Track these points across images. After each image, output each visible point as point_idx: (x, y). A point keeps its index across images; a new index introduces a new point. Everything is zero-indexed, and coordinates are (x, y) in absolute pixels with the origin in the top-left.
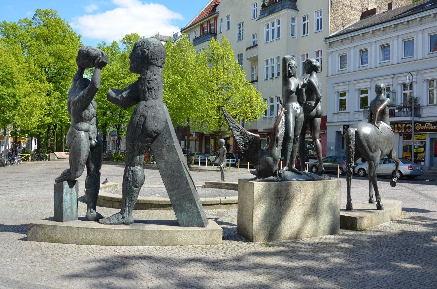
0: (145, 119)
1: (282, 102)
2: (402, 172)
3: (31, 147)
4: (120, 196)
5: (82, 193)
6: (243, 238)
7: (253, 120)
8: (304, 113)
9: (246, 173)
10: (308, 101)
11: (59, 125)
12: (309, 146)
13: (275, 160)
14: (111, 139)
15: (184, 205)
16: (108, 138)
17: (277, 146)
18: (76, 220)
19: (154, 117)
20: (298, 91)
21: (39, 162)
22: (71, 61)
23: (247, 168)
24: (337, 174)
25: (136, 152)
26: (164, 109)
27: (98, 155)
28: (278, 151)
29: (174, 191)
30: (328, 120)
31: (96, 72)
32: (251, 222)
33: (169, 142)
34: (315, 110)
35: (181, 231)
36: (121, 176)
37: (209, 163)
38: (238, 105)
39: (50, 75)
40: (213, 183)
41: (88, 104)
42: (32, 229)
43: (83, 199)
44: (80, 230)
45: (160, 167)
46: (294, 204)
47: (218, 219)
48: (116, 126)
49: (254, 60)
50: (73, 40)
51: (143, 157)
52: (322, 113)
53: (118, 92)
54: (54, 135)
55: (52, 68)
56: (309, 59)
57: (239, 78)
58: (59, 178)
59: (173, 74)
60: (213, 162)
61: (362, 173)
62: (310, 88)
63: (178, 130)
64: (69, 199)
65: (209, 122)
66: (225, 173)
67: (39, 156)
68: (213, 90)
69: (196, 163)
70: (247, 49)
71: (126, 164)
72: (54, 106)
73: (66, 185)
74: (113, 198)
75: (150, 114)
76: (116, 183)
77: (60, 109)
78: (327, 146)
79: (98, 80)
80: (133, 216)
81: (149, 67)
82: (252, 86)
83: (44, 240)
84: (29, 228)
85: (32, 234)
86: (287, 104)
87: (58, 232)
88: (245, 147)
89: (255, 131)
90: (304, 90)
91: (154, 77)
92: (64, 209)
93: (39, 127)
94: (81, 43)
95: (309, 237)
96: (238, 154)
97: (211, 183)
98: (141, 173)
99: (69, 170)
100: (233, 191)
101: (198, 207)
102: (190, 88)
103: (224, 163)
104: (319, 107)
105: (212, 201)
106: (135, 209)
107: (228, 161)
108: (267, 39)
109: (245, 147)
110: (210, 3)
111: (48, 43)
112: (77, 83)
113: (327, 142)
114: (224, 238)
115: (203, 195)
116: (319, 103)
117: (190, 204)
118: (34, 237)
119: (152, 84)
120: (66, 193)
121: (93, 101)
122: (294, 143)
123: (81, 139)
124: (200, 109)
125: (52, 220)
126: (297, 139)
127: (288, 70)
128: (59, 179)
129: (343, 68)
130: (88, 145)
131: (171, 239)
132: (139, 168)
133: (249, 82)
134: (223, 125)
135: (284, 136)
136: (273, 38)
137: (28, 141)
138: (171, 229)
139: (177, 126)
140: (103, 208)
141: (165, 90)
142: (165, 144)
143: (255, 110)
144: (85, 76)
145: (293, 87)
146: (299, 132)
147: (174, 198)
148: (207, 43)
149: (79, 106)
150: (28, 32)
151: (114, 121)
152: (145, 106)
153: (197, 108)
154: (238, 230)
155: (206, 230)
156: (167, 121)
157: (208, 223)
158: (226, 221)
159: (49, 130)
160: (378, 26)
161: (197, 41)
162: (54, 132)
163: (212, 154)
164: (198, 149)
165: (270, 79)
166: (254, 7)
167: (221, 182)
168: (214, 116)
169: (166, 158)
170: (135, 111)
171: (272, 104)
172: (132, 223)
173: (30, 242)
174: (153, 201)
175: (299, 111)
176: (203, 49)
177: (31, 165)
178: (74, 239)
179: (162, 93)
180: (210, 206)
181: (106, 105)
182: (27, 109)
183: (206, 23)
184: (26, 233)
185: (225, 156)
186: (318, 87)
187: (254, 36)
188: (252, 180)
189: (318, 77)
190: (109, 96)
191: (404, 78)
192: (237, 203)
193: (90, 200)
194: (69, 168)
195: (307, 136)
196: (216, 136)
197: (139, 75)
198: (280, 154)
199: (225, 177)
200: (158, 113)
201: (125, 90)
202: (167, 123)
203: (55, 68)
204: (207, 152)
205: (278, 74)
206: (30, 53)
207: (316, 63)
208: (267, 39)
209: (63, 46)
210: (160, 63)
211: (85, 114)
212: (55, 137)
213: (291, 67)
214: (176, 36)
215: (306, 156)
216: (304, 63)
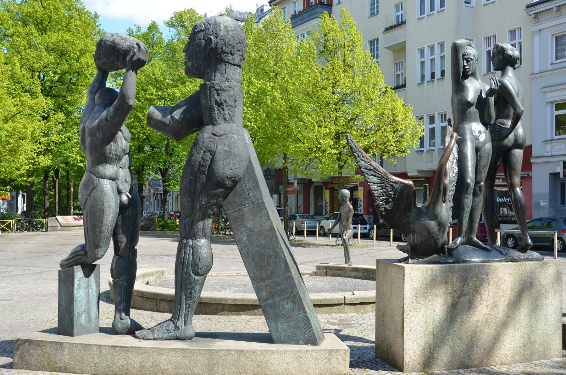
0: (214, 156)
1: (452, 123)
3: (17, 208)
4: (171, 291)
5: (104, 287)
6: (387, 365)
7: (399, 155)
8: (492, 141)
9: (391, 250)
10: (500, 120)
11: (64, 170)
12: (501, 200)
13: (441, 225)
14: (152, 193)
15: (281, 308)
16: (147, 191)
17: (444, 201)
19: (228, 153)
20: (481, 103)
21: (31, 233)
22: (83, 60)
23: (389, 240)
24: (553, 250)
25: (198, 214)
26: (245, 139)
27: (132, 222)
28: (446, 209)
29: (263, 281)
30: (534, 153)
31: (128, 77)
32: (400, 336)
33: (254, 196)
34: (511, 136)
35: (277, 352)
36: (140, 255)
37: (322, 232)
38: (371, 129)
39: (48, 84)
40: (331, 268)
41: (115, 134)
42: (21, 349)
43: (103, 297)
44: (103, 350)
45: (240, 240)
46: (477, 304)
47: (341, 331)
48: (160, 170)
49: (399, 50)
50: (85, 22)
51: (209, 222)
52: (524, 140)
53: (164, 111)
54: (54, 187)
55: (50, 72)
56: (500, 44)
57: (373, 81)
58: (66, 260)
59: (257, 77)
60: (329, 230)
62: (503, 97)
63: (267, 173)
64: (84, 296)
65: (320, 160)
66: (351, 250)
67: (29, 222)
68: (328, 104)
69: (300, 233)
70: (387, 30)
71: (181, 235)
72: (55, 138)
73: (79, 273)
74: (158, 295)
75: (221, 148)
76: (161, 269)
77: (64, 143)
78: (534, 200)
79: (132, 91)
80: (193, 325)
81: (219, 66)
82: (395, 95)
84: (16, 346)
85: (22, 357)
86: (460, 126)
87: (66, 353)
88: (387, 203)
89: (404, 175)
90: (492, 99)
91: (227, 84)
92: (75, 313)
93: (30, 174)
94: (98, 26)
95: (504, 364)
96: (372, 216)
97: (326, 268)
98: (206, 251)
99: (83, 247)
100: (367, 281)
101: (307, 309)
102: (287, 101)
103: (350, 232)
104: (520, 130)
105: (329, 300)
106: (197, 313)
107: (355, 228)
108: (422, 12)
109: (387, 203)
111: (43, 30)
112: (97, 97)
113: (533, 192)
114: (353, 365)
115: (314, 289)
116: (519, 124)
117: (292, 305)
118: (24, 363)
119: (224, 96)
120: (79, 285)
121: (123, 128)
122: (475, 194)
123: (103, 192)
124: (304, 138)
125: (55, 333)
126: (480, 187)
127: (461, 66)
128: (67, 262)
129: (561, 58)
130: (116, 204)
131: (259, 366)
132: (203, 242)
133: (391, 89)
134: (346, 166)
135: (457, 182)
136: (432, 9)
137: (12, 197)
138: (260, 349)
139: (266, 168)
140: (140, 311)
141: (244, 105)
142: (247, 199)
143: (402, 137)
144: (108, 85)
145: (471, 96)
146: (484, 175)
147: (264, 294)
148: (314, 22)
149: (99, 136)
150: (8, 10)
151: (158, 159)
152: (213, 134)
153: (299, 136)
154: (376, 350)
155: (321, 351)
156: (250, 160)
157: (324, 338)
158: (355, 333)
159: (46, 178)
161: (297, 19)
162: (54, 182)
163: (327, 216)
164: (302, 207)
165: (428, 82)
167: (344, 265)
168: (329, 149)
169: (249, 224)
170: (196, 144)
171: (432, 126)
172: (191, 339)
173: (18, 371)
174: (227, 300)
175: (483, 138)
176: (309, 33)
177: (17, 238)
178: (92, 365)
179: (241, 111)
180: (327, 308)
181: (144, 133)
182: (9, 143)
184: (11, 355)
185: (350, 220)
186: (518, 94)
187: (398, 7)
188: (400, 261)
189: (516, 75)
190: (150, 118)
192: (374, 303)
193: (119, 298)
194: (84, 243)
195: (498, 182)
196: (333, 184)
197: (200, 81)
198: (451, 214)
199: (351, 257)
200: (235, 147)
201: (178, 107)
202: (250, 163)
203: (55, 73)
204: (319, 212)
205: (443, 73)
206: (13, 48)
207: (513, 52)
208: (422, 12)
209: (69, 34)
210: (237, 59)
211: (111, 150)
212: (57, 191)
214: (262, 11)
215: (496, 219)
216: (488, 52)
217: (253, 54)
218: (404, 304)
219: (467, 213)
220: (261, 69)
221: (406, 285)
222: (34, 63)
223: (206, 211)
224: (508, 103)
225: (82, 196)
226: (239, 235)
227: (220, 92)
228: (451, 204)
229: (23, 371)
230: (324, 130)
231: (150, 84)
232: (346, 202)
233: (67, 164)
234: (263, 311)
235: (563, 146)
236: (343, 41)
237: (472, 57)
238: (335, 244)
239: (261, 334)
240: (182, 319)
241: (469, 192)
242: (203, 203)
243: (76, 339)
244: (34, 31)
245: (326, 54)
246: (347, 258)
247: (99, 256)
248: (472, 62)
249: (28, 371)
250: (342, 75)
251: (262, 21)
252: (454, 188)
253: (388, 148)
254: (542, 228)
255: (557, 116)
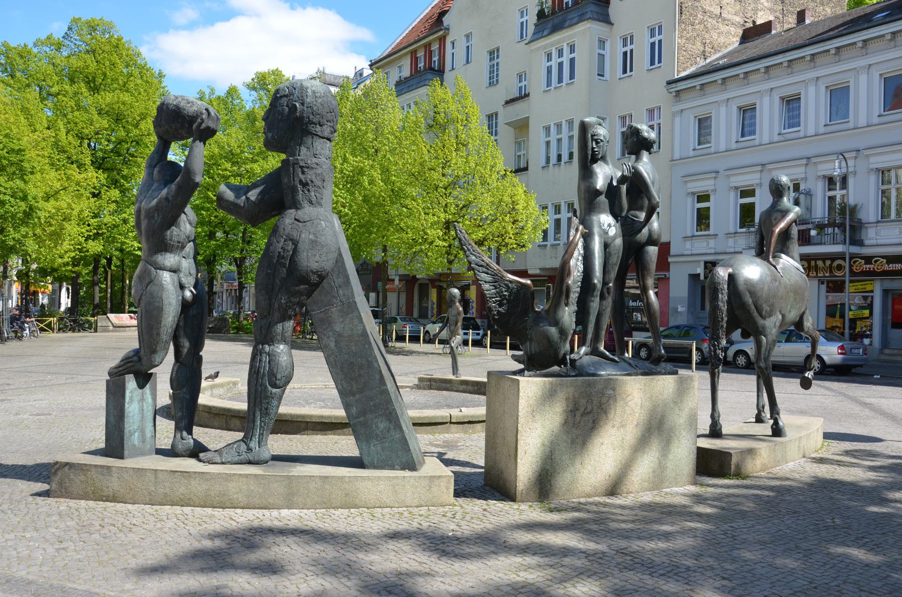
0: (296, 246)
1: (578, 214)
2: (825, 358)
3: (60, 304)
4: (243, 406)
5: (163, 400)
6: (497, 494)
7: (519, 250)
9: (504, 360)
10: (632, 212)
12: (634, 304)
13: (563, 332)
15: (374, 426)
16: (218, 285)
17: (567, 305)
18: (151, 454)
19: (314, 243)
20: (612, 191)
22: (143, 125)
23: (505, 349)
24: (690, 362)
25: (277, 315)
26: (334, 227)
27: (198, 321)
29: (354, 395)
30: (673, 251)
32: (513, 460)
33: (344, 295)
34: (645, 231)
35: (368, 478)
38: (487, 218)
39: (100, 154)
40: (435, 380)
42: (60, 473)
43: (165, 412)
44: (160, 475)
45: (326, 346)
47: (445, 454)
49: (522, 126)
50: (147, 82)
51: (290, 324)
52: (659, 236)
53: (239, 190)
54: (106, 279)
55: (103, 140)
56: (634, 124)
57: (490, 162)
58: (115, 368)
61: (741, 360)
62: (636, 185)
63: (363, 269)
64: (136, 411)
65: (426, 254)
67: (75, 321)
69: (401, 338)
70: (507, 102)
71: (256, 339)
72: (108, 219)
73: (131, 383)
74: (229, 410)
75: (305, 237)
76: (234, 380)
78: (671, 305)
79: (198, 166)
82: (516, 180)
83: (86, 497)
84: (53, 470)
85: (61, 484)
86: (587, 218)
87: (114, 479)
88: (500, 305)
89: (523, 274)
90: (624, 188)
91: (314, 160)
92: (126, 431)
93: (75, 262)
94: (163, 88)
96: (486, 321)
97: (430, 380)
99: (137, 352)
100: (477, 396)
101: (404, 428)
103: (458, 339)
104: (655, 224)
106: (273, 432)
107: (465, 334)
108: (549, 84)
109: (500, 305)
110: (430, 8)
111: (95, 89)
113: (671, 295)
114: (458, 494)
115: (414, 405)
116: (655, 217)
117: (387, 423)
119: (310, 175)
120: (131, 398)
121: (188, 209)
122: (602, 297)
123: (161, 287)
124: (408, 228)
126: (608, 289)
127: (590, 148)
128: (116, 370)
130: (178, 301)
131: (347, 495)
134: (456, 261)
136: (560, 80)
140: (206, 430)
141: (336, 186)
143: (522, 228)
144: (171, 157)
145: (600, 183)
147: (354, 410)
148: (423, 90)
149: (158, 218)
151: (232, 250)
153: (402, 225)
154: (485, 477)
155: (420, 477)
157: (424, 462)
158: (462, 457)
159: (96, 269)
160: (775, 58)
161: (402, 86)
162: (106, 272)
163: (434, 319)
164: (404, 308)
165: (554, 165)
166: (522, 17)
168: (437, 240)
170: (275, 231)
171: (558, 216)
172: (266, 462)
173: (56, 499)
174: (311, 416)
175: (612, 232)
176: (416, 103)
177: (60, 340)
180: (429, 428)
181: (216, 217)
182: (51, 225)
183: (423, 49)
184: (48, 480)
185: (459, 324)
186: (653, 183)
187: (521, 76)
188: (515, 373)
189: (652, 161)
190: (220, 199)
191: (829, 166)
192: (484, 421)
193: (180, 414)
194: (138, 347)
196: (440, 282)
197: (283, 156)
198: (574, 319)
199: (459, 368)
200: (322, 235)
201: (254, 186)
202: (340, 255)
203: (109, 141)
204: (423, 315)
205: (571, 155)
206: (58, 109)
208: (549, 84)
211: (171, 236)
212: (109, 283)
213: (596, 140)
214: (361, 75)
217: (349, 126)
218: (517, 423)
219: (592, 319)
220: (360, 144)
221: (520, 401)
222: (83, 128)
223: (286, 311)
224: (642, 192)
225: (136, 291)
226: (325, 340)
227: (306, 170)
228: (574, 308)
229: (62, 500)
230: (432, 219)
231: (225, 157)
232: (455, 303)
233: (121, 250)
234: (353, 430)
235: (897, 231)
236: (455, 114)
237: (602, 138)
238: (441, 352)
239: (351, 457)
240: (256, 439)
241: (595, 294)
242: (283, 301)
243: (128, 463)
244: (84, 90)
245: (436, 129)
246: (455, 368)
247: (156, 363)
248: (602, 144)
249: (68, 500)
250: (454, 154)
251: (362, 86)
252: (579, 289)
253: (506, 241)
254: (679, 337)
255: (698, 209)
